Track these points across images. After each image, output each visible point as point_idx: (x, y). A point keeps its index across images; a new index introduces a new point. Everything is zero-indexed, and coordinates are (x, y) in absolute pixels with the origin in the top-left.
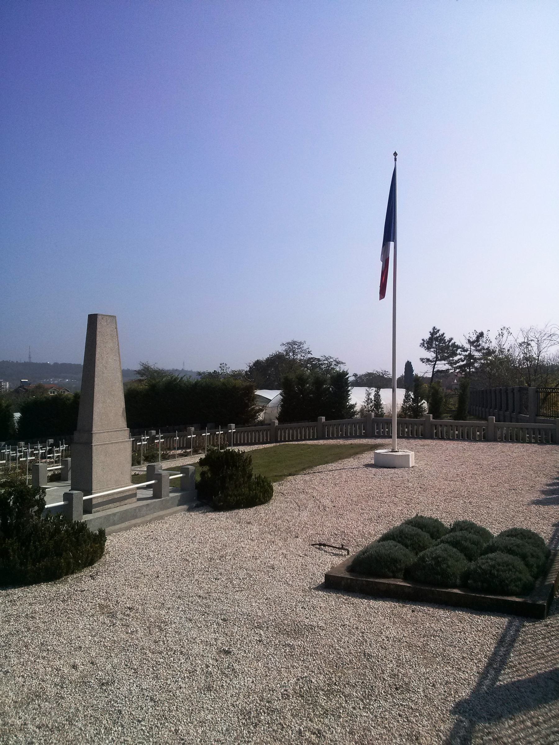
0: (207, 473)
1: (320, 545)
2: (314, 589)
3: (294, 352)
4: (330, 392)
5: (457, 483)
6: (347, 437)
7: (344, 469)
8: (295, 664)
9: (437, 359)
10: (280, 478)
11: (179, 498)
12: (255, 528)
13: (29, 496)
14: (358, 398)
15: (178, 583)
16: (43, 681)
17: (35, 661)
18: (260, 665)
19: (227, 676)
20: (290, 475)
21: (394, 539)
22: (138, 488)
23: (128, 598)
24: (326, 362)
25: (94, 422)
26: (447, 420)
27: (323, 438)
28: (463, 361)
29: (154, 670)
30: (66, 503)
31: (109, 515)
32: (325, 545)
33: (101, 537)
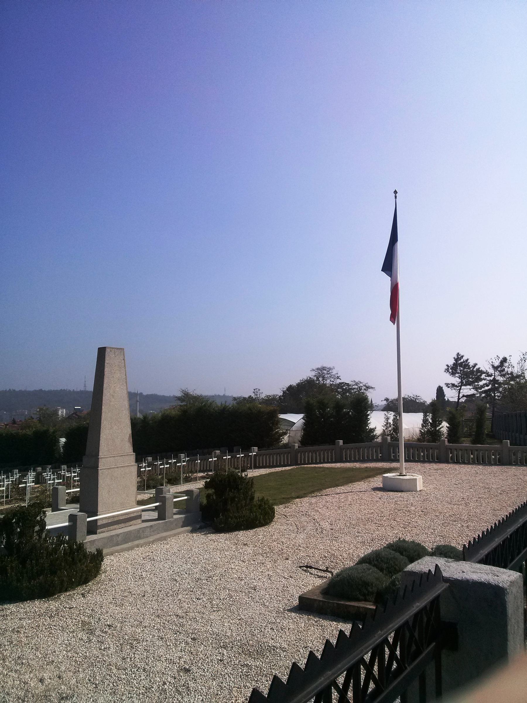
0: (212, 496)
1: (307, 567)
2: (288, 610)
3: (323, 378)
4: (350, 416)
5: (461, 507)
6: (363, 461)
7: (351, 492)
8: (248, 684)
9: (462, 384)
10: (286, 500)
11: (183, 520)
12: (249, 550)
13: (29, 518)
14: (377, 422)
15: (161, 602)
16: (8, 694)
17: (7, 674)
18: (214, 683)
19: (180, 693)
20: (298, 497)
21: (370, 563)
22: (143, 510)
23: (111, 616)
24: (356, 387)
25: (100, 448)
26: (466, 443)
27: (341, 461)
28: (488, 386)
29: (114, 685)
30: (71, 524)
31: (112, 536)
32: (311, 567)
33: (98, 557)
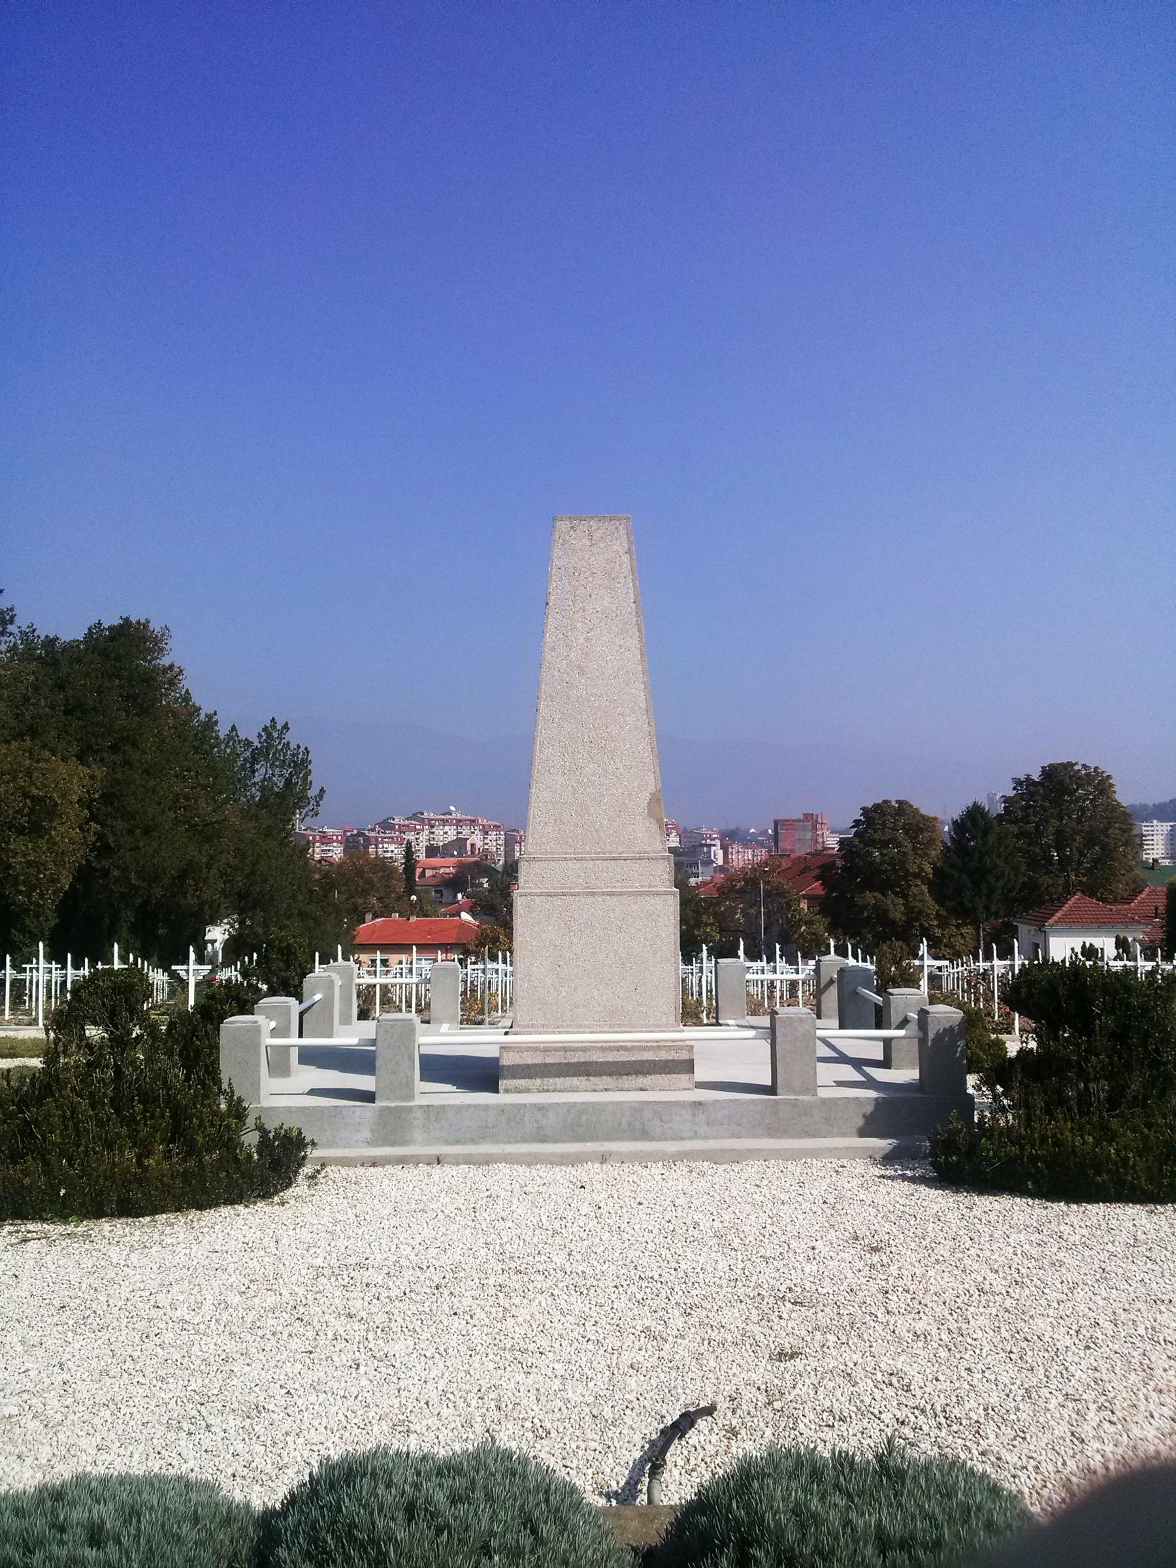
11: (869, 1109)
